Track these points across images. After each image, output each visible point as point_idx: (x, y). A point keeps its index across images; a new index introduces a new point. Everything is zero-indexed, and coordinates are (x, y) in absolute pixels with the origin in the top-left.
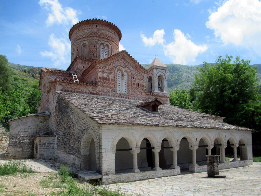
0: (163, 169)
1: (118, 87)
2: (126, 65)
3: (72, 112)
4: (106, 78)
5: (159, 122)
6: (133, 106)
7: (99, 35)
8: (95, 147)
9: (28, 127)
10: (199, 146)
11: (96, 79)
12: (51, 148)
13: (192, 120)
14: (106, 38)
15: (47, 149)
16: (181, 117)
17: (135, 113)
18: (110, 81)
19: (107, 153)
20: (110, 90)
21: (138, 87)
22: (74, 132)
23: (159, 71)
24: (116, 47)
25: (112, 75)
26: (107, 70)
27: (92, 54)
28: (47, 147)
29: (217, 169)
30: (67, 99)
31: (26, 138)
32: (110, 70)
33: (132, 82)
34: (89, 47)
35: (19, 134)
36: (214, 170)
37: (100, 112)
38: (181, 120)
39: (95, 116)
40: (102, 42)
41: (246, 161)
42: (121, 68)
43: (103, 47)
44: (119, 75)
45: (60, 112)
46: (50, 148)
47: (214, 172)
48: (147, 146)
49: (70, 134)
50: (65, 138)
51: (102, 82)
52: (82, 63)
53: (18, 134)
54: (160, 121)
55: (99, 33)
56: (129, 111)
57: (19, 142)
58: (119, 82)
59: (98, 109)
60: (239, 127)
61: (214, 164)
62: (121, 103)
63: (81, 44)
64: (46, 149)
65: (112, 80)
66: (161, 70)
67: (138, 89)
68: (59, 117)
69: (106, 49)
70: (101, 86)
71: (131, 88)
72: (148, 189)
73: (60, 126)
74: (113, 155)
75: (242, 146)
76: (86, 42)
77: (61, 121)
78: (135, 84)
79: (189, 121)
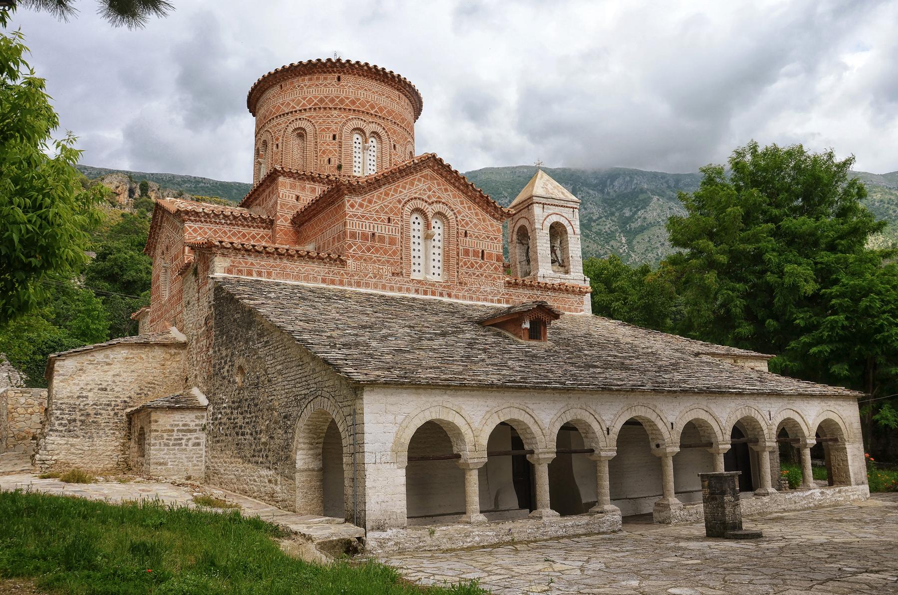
0: (563, 514)
1: (413, 261)
2: (439, 197)
3: (265, 339)
4: (373, 234)
5: (549, 374)
6: (466, 323)
7: (347, 105)
9: (114, 376)
10: (682, 446)
11: (339, 236)
12: (190, 443)
13: (660, 367)
14: (372, 112)
15: (177, 448)
16: (625, 358)
17: (470, 345)
18: (387, 245)
19: (380, 466)
20: (387, 270)
21: (480, 261)
22: (270, 398)
23: (551, 212)
24: (406, 139)
26: (377, 211)
27: (326, 160)
28: (176, 439)
29: (734, 513)
30: (246, 301)
31: (104, 409)
32: (386, 213)
33: (461, 248)
34: (316, 137)
35: (83, 397)
36: (723, 513)
37: (357, 344)
38: (624, 367)
39: (339, 356)
41: (844, 488)
43: (360, 140)
44: (416, 226)
45: (222, 338)
46: (186, 445)
47: (724, 523)
48: (509, 441)
49: (256, 405)
50: (241, 417)
51: (359, 248)
52: (293, 187)
53: (79, 397)
54: (552, 372)
55: (348, 98)
56: (451, 339)
57: (82, 422)
58: (417, 247)
59: (350, 334)
60: (818, 385)
61: (723, 499)
62: (423, 312)
63: (290, 129)
64: (174, 445)
65: (392, 241)
66: (557, 210)
67: (481, 267)
68: (219, 350)
69: (373, 142)
70: (357, 259)
71: (458, 264)
72: (509, 569)
73: (224, 378)
74: (399, 470)
75: (830, 443)
76: (303, 124)
77: (225, 363)
78: (471, 254)
79: (648, 371)
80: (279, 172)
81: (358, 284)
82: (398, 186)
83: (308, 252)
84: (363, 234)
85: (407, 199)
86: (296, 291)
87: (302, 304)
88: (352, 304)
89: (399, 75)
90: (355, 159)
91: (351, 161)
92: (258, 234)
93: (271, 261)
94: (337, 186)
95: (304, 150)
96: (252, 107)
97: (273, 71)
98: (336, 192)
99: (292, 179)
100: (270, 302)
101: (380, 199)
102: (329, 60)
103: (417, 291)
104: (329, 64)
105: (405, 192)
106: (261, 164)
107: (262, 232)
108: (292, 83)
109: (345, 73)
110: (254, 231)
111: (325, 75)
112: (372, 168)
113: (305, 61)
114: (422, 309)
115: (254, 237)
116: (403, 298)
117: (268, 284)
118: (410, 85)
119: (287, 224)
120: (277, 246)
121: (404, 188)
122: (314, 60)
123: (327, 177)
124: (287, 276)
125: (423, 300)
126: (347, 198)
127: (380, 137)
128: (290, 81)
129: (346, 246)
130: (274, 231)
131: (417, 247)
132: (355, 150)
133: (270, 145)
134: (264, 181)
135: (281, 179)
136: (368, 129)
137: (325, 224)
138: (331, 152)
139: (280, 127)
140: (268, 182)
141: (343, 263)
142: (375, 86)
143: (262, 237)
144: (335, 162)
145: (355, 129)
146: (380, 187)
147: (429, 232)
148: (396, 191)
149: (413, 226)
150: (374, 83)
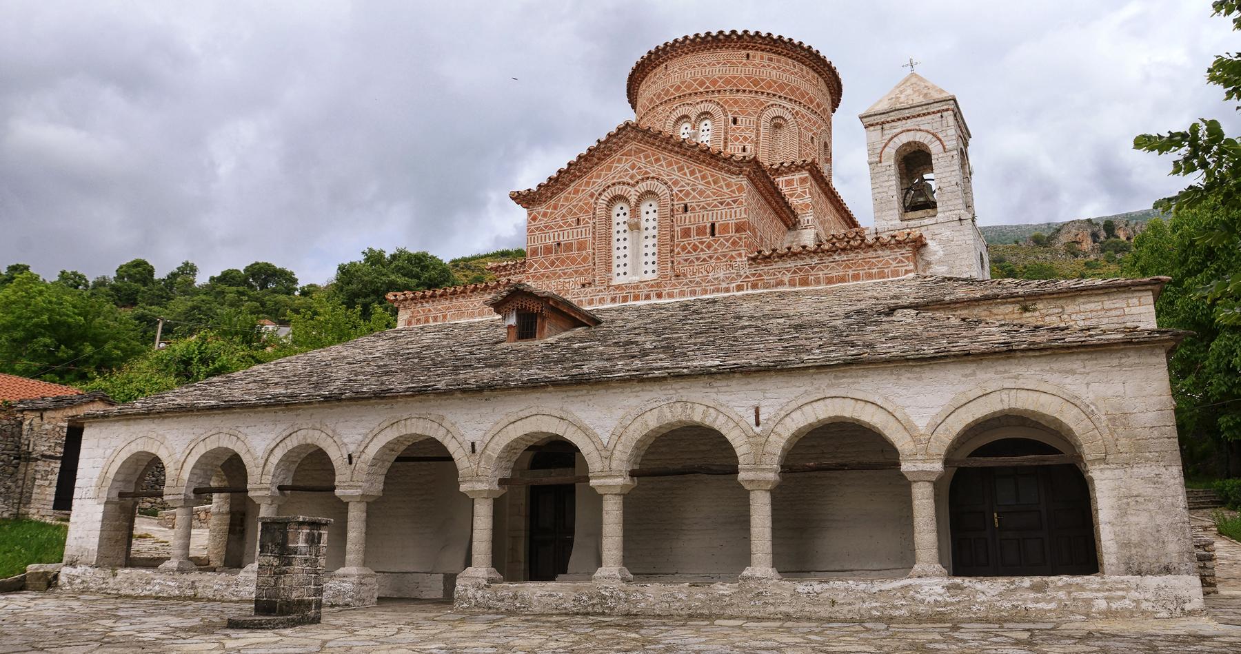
2: (646, 173)
8: (710, 580)
21: (708, 239)
25: (581, 228)
33: (677, 229)
40: (679, 113)
42: (618, 190)
66: (901, 126)
67: (709, 247)
71: (672, 251)
124: (461, 315)
142: (708, 57)
145: (680, 119)
150: (707, 54)
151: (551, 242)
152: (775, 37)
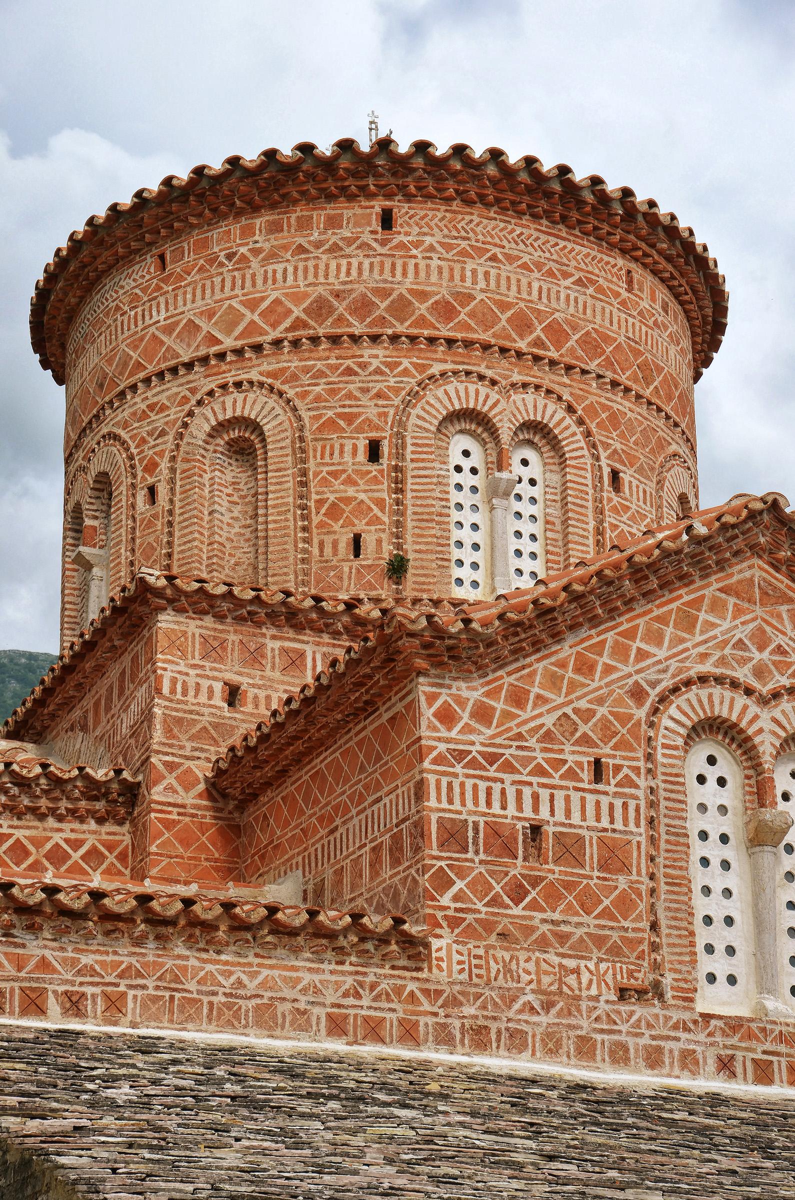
1: (703, 936)
4: (536, 830)
7: (422, 322)
11: (397, 839)
20: (595, 977)
24: (662, 444)
26: (548, 736)
27: (345, 539)
32: (585, 740)
34: (301, 453)
40: (462, 394)
43: (476, 459)
44: (710, 794)
51: (480, 886)
52: (213, 650)
55: (422, 296)
58: (718, 880)
62: (755, 1158)
63: (201, 427)
65: (614, 858)
69: (529, 465)
70: (470, 933)
76: (251, 405)
80: (158, 593)
81: (480, 1038)
82: (631, 634)
83: (356, 917)
84: (494, 830)
85: (667, 683)
86: (220, 1072)
87: (243, 1124)
88: (450, 1122)
89: (627, 193)
90: (456, 534)
91: (443, 542)
92: (76, 844)
93: (124, 954)
94: (384, 641)
95: (255, 506)
96: (52, 347)
97: (126, 200)
98: (384, 663)
99: (209, 621)
100: (108, 1120)
101: (550, 689)
102: (346, 146)
103: (726, 1066)
104: (345, 163)
105: (661, 654)
106: (88, 566)
107: (92, 834)
108: (204, 244)
109: (409, 198)
110: (58, 834)
111: (331, 209)
112: (527, 565)
113: (251, 155)
114: (748, 1144)
115: (57, 857)
116: (671, 1096)
117: (108, 1047)
118: (671, 230)
119: (191, 798)
120: (149, 886)
121: (658, 639)
122: (286, 150)
123: (350, 606)
124: (189, 1011)
125: (755, 1106)
126: (424, 686)
127: (554, 443)
128: (196, 235)
129: (425, 881)
130: (140, 833)
131: (718, 880)
132: (455, 497)
133: (122, 491)
134: (100, 632)
135: (166, 621)
136: (509, 411)
137: (342, 793)
138: (361, 509)
139: (159, 420)
140: (114, 636)
141: (415, 950)
143: (93, 856)
144: (379, 548)
145: (455, 416)
146: (557, 637)
147: (767, 814)
148: (621, 652)
149: (696, 794)
150: (527, 229)
151: (514, 815)
152: (403, 147)
